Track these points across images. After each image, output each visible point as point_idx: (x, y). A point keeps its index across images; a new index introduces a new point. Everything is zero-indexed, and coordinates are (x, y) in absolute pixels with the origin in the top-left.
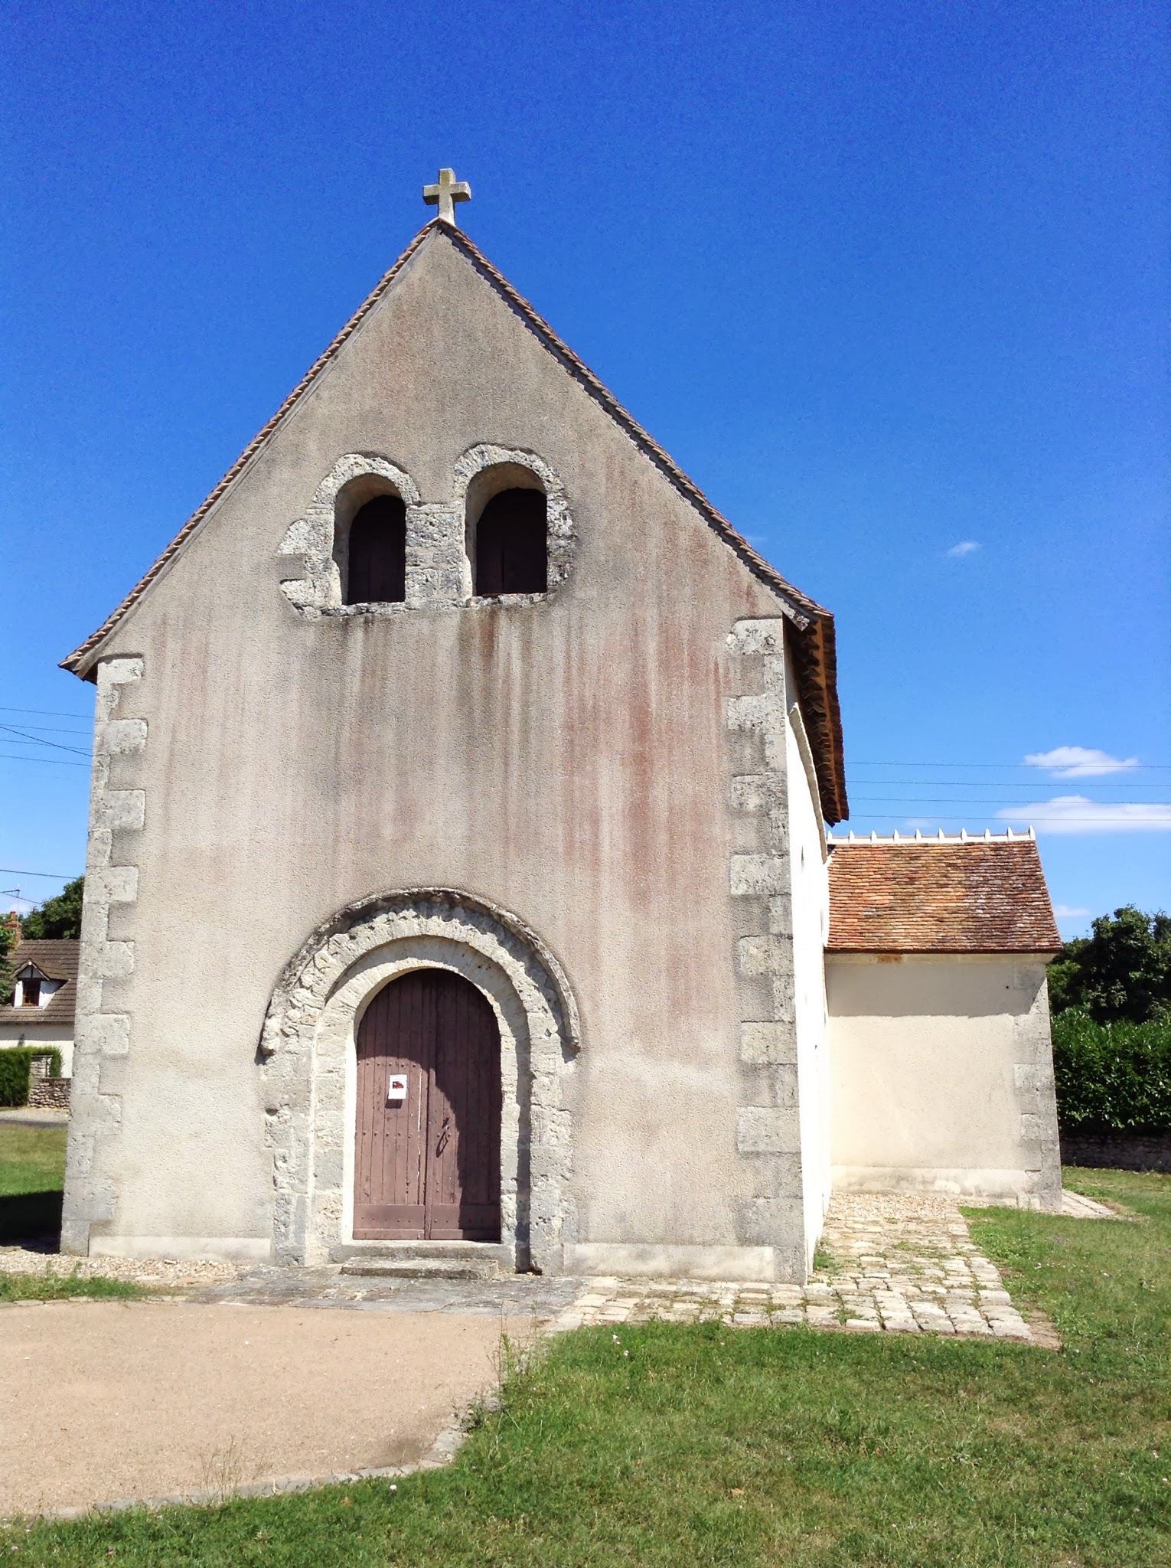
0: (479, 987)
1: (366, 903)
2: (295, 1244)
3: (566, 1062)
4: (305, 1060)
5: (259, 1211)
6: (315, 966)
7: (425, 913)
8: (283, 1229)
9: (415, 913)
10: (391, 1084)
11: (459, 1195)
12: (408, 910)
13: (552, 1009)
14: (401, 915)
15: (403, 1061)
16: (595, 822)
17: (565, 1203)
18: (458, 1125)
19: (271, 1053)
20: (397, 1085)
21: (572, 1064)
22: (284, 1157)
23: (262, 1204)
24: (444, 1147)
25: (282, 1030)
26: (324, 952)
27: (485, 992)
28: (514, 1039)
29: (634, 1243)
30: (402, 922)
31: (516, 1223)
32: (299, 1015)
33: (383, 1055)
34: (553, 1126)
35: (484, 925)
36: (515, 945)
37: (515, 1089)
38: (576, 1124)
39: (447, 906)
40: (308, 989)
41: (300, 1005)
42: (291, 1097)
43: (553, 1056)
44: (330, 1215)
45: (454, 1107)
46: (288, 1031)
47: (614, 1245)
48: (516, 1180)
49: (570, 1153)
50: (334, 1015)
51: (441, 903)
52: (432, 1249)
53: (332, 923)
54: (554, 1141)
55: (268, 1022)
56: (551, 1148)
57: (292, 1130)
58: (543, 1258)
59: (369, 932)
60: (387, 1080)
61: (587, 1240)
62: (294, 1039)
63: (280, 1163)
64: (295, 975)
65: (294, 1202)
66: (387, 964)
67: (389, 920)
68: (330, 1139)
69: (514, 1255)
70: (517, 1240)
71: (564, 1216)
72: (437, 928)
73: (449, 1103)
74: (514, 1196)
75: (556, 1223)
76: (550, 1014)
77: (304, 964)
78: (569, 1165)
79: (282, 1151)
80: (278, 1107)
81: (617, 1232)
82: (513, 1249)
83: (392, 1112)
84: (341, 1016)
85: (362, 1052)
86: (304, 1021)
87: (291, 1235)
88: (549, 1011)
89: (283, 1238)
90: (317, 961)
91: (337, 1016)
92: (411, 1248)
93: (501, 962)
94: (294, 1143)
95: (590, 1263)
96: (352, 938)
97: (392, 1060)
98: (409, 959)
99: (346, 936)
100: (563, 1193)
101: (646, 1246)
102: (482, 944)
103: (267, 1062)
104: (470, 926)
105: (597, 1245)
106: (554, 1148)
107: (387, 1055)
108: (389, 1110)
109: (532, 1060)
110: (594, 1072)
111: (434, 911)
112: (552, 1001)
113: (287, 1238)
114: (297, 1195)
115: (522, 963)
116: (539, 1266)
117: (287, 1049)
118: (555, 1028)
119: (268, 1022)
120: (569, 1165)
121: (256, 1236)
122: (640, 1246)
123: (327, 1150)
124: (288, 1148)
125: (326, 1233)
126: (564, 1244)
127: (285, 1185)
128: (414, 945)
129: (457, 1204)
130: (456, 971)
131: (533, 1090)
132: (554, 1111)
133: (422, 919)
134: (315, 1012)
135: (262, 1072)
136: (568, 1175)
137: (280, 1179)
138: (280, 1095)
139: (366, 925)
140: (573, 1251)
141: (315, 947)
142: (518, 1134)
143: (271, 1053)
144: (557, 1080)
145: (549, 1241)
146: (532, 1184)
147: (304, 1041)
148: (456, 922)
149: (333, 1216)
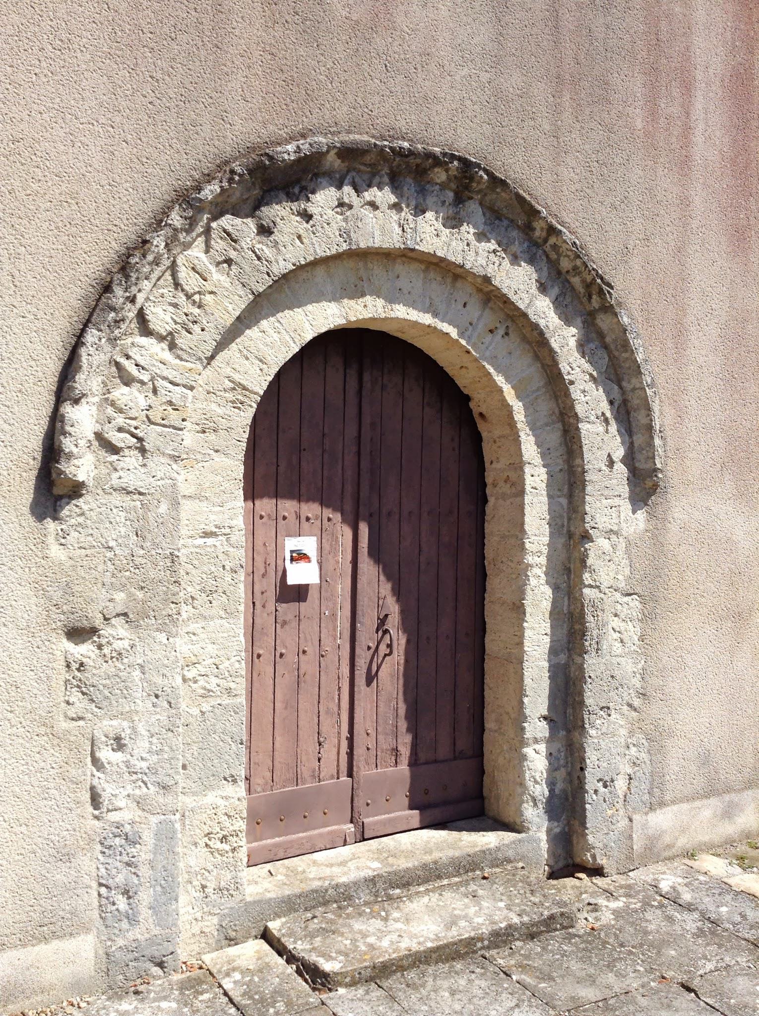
0: (491, 370)
1: (306, 149)
2: (156, 931)
3: (634, 512)
4: (163, 508)
5: (60, 875)
6: (177, 285)
7: (413, 203)
8: (122, 903)
9: (393, 199)
10: (288, 557)
11: (405, 752)
12: (380, 188)
13: (616, 419)
14: (368, 195)
15: (311, 509)
16: (688, 88)
17: (633, 750)
18: (405, 625)
19: (76, 490)
20: (299, 557)
21: (641, 515)
22: (118, 739)
23: (65, 857)
24: (379, 668)
25: (99, 436)
26: (197, 252)
27: (500, 380)
28: (544, 470)
29: (719, 794)
30: (367, 212)
31: (547, 793)
32: (143, 403)
33: (270, 497)
34: (616, 623)
35: (516, 248)
36: (562, 294)
37: (543, 560)
38: (647, 618)
39: (450, 195)
40: (161, 338)
41: (145, 377)
42: (130, 595)
43: (617, 501)
44: (219, 845)
45: (398, 592)
46: (117, 438)
47: (698, 803)
48: (545, 718)
49: (640, 666)
50: (214, 406)
51: (443, 186)
52: (416, 868)
53: (225, 184)
54: (617, 648)
55: (68, 410)
56: (615, 660)
57: (137, 673)
58: (606, 846)
59: (296, 224)
60: (278, 547)
61: (662, 804)
62: (131, 459)
63: (105, 754)
64: (133, 300)
65: (148, 837)
66: (325, 304)
67: (341, 204)
68: (214, 681)
69: (544, 845)
70: (549, 820)
71: (630, 771)
72: (436, 240)
73: (389, 586)
74: (542, 747)
75: (621, 784)
76: (613, 427)
77: (154, 276)
78: (638, 685)
79: (109, 726)
80: (98, 622)
81: (699, 783)
82: (543, 836)
83: (288, 610)
84: (229, 410)
85: (252, 492)
86: (155, 416)
87: (145, 913)
88: (613, 422)
89: (125, 925)
90: (183, 273)
91: (220, 411)
92: (380, 876)
93: (542, 323)
94: (143, 704)
95: (667, 839)
96: (265, 231)
97: (288, 507)
98: (368, 299)
99: (250, 225)
100: (631, 733)
101: (734, 797)
102: (514, 286)
103: (65, 512)
104: (493, 245)
105: (675, 808)
106: (619, 659)
107: (277, 495)
108: (282, 607)
109: (587, 508)
110: (674, 529)
111: (430, 200)
112: (616, 404)
113: (132, 919)
114: (154, 820)
115: (573, 330)
116: (599, 861)
117: (115, 482)
118: (619, 453)
119: (68, 410)
120: (638, 685)
121: (55, 935)
122: (727, 797)
123: (206, 707)
124: (128, 716)
125: (211, 886)
126: (634, 817)
127: (121, 803)
128: (377, 269)
129: (404, 767)
130: (454, 333)
131: (589, 562)
132: (618, 595)
133: (406, 214)
134: (184, 397)
135: (51, 540)
136: (637, 702)
137: (107, 790)
138: (103, 594)
139: (295, 206)
140: (645, 826)
141: (182, 236)
142: (547, 639)
143: (76, 490)
144: (622, 545)
145: (612, 816)
146: (587, 726)
147: (159, 465)
148: (468, 231)
149: (227, 847)
